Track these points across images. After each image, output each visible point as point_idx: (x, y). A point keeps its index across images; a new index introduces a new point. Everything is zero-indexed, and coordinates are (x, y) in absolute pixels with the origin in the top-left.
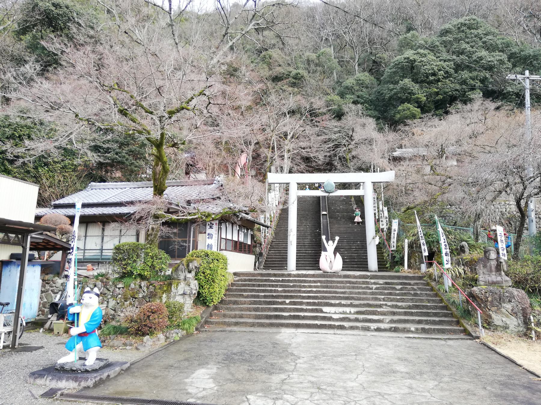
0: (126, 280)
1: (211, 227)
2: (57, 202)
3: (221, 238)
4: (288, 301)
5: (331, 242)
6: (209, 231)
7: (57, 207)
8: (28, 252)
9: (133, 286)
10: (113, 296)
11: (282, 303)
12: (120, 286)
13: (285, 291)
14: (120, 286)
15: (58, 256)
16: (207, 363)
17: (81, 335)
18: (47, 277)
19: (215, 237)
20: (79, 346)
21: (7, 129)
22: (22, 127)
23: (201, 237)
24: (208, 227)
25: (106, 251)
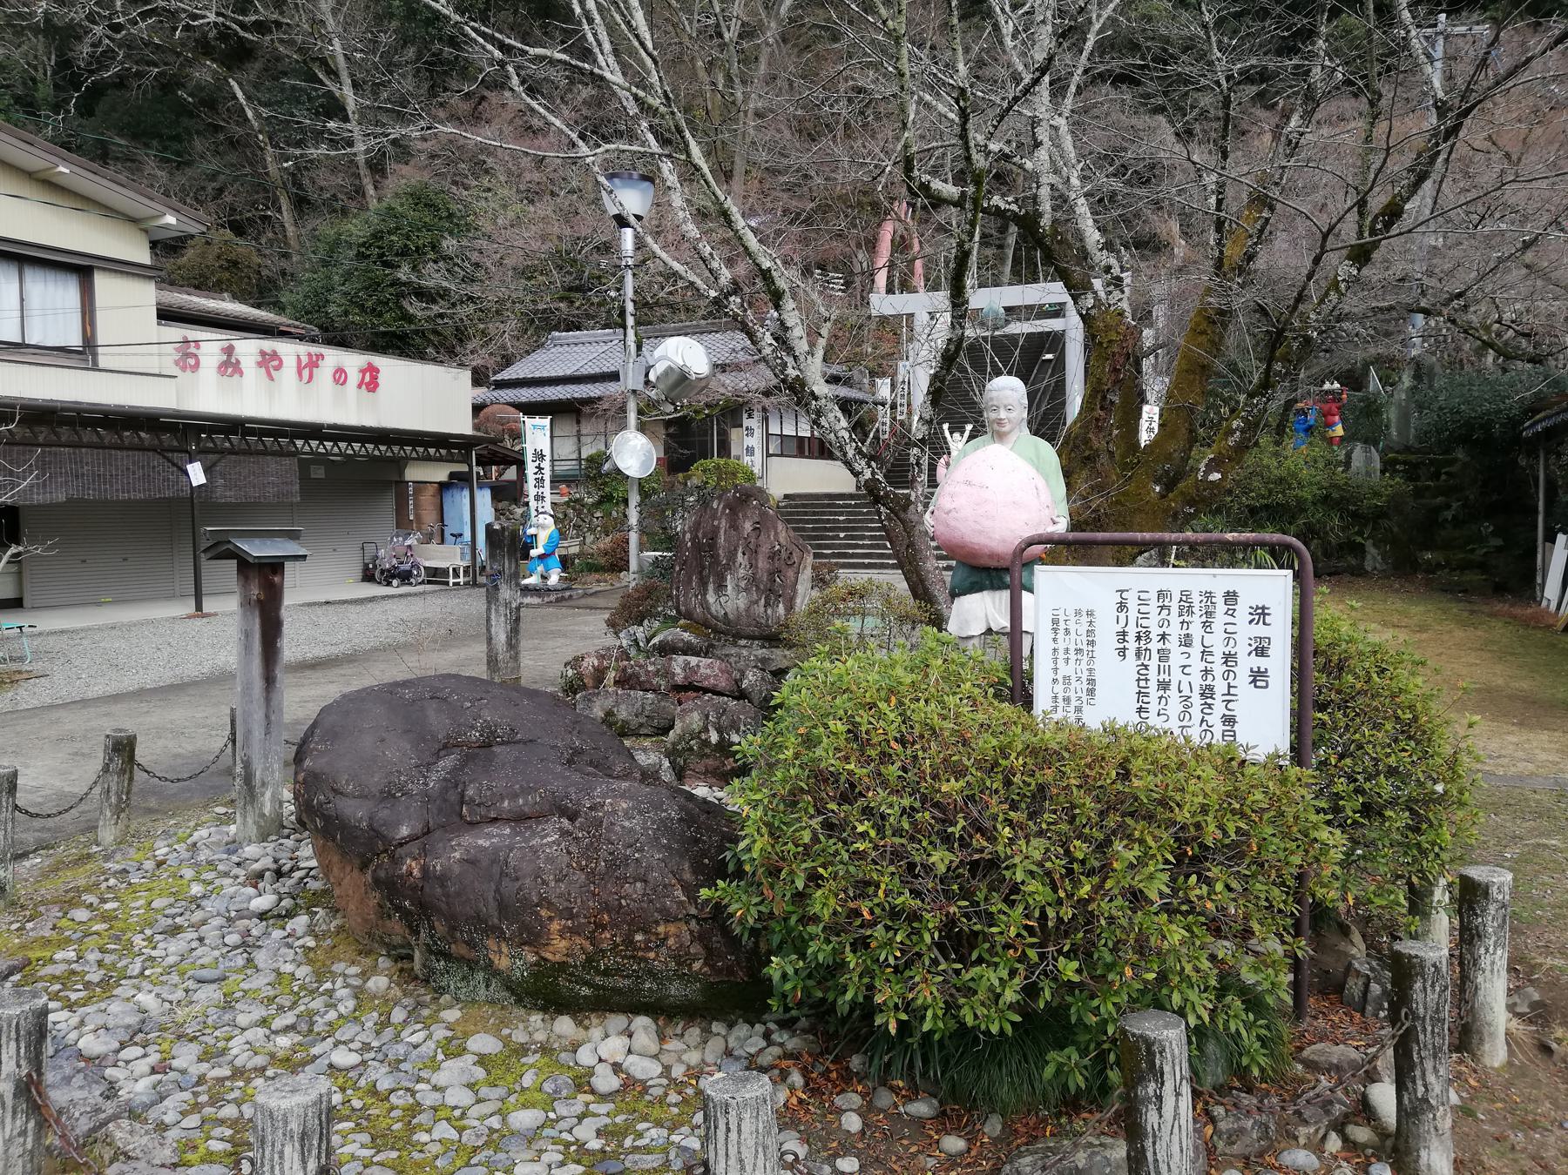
0: (606, 506)
1: (750, 416)
2: (499, 377)
3: (768, 435)
4: (842, 535)
5: (957, 435)
6: (746, 422)
7: (501, 385)
8: (475, 469)
9: (614, 514)
10: (589, 529)
11: (833, 538)
12: (598, 514)
13: (849, 521)
14: (598, 514)
15: (511, 474)
16: (222, 291)
17: (541, 557)
18: (500, 506)
19: (758, 433)
20: (540, 569)
21: (394, 238)
22: (419, 230)
23: (734, 434)
24: (745, 416)
25: (467, 501)
